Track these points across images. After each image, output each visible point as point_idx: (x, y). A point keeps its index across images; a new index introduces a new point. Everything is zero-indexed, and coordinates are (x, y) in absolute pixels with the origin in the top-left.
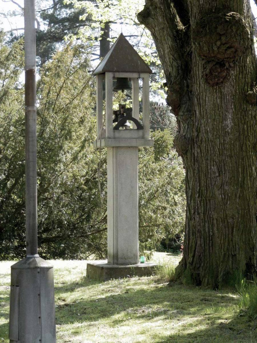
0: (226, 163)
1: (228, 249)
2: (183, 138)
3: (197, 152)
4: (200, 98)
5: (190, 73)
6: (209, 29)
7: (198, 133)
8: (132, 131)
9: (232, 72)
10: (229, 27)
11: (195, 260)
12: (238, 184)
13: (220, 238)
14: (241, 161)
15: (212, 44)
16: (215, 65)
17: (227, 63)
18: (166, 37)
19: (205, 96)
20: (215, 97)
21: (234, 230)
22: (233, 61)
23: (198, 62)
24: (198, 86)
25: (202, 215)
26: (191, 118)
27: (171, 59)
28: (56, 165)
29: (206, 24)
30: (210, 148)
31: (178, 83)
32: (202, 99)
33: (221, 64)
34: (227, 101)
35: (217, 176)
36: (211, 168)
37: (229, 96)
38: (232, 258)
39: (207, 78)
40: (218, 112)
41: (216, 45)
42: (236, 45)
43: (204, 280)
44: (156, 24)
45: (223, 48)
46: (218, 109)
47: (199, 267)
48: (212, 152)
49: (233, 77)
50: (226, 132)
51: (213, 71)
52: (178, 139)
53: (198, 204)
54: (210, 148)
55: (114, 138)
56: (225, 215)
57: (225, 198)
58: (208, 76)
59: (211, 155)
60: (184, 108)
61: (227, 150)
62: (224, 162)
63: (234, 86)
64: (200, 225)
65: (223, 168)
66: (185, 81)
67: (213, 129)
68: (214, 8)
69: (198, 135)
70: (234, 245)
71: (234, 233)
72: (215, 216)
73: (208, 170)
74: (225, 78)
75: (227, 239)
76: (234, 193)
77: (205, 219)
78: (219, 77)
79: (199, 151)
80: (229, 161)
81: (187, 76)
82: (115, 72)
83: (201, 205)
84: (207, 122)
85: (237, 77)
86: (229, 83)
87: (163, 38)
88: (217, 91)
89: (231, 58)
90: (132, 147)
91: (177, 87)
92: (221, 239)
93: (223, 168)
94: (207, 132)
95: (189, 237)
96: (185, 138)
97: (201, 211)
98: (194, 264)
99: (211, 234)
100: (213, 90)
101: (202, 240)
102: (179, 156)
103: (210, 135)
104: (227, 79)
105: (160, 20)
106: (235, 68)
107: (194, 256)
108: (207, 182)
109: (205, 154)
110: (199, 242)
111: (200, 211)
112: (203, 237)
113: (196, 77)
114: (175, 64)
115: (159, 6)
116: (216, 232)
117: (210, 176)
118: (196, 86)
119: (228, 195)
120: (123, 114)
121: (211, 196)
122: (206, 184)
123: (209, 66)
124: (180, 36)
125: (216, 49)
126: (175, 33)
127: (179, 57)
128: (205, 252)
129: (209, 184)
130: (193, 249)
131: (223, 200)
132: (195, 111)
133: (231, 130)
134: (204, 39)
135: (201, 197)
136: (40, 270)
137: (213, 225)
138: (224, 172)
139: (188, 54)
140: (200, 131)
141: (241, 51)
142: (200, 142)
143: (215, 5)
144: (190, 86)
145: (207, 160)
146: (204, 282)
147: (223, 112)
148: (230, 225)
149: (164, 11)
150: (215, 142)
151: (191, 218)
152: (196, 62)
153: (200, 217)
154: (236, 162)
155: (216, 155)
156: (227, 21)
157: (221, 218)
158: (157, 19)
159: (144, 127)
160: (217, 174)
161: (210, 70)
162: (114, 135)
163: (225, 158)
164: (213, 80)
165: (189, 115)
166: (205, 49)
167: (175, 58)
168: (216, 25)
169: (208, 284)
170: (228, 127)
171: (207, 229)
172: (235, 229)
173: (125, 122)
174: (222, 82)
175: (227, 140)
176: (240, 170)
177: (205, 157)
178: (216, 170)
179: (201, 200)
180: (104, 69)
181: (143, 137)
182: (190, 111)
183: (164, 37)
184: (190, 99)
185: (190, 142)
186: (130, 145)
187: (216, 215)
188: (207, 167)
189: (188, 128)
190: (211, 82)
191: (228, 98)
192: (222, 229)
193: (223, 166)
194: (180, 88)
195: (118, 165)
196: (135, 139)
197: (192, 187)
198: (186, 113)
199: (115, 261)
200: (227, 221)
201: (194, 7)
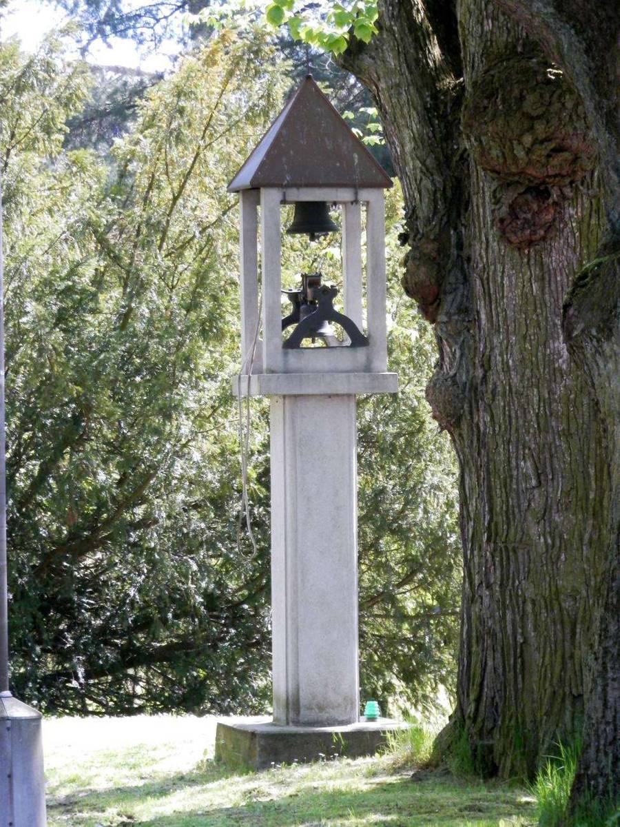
0: (556, 452)
1: (561, 680)
2: (450, 383)
3: (485, 422)
4: (488, 279)
5: (466, 210)
6: (504, 101)
7: (486, 372)
8: (337, 352)
9: (571, 212)
10: (555, 96)
11: (482, 708)
12: (587, 508)
13: (542, 650)
14: (593, 445)
15: (511, 141)
16: (524, 193)
17: (555, 188)
18: (405, 110)
19: (500, 274)
20: (526, 277)
21: (578, 630)
22: (571, 183)
23: (481, 184)
24: (484, 246)
25: (498, 589)
26: (468, 331)
27: (418, 171)
28: (168, 417)
29: (497, 89)
30: (516, 412)
31: (432, 237)
32: (495, 281)
33: (540, 191)
34: (557, 287)
35: (534, 488)
36: (517, 466)
37: (561, 275)
38: (573, 704)
39: (504, 227)
40: (534, 317)
41: (520, 143)
42: (575, 143)
43: (502, 762)
44: (382, 75)
45: (541, 151)
46: (535, 310)
47: (493, 728)
48: (521, 422)
49: (574, 225)
50: (554, 369)
51: (520, 208)
52: (435, 385)
53: (487, 561)
54: (516, 412)
55: (286, 372)
56: (553, 589)
57: (553, 545)
58: (505, 223)
59: (517, 430)
60: (449, 303)
61: (557, 418)
62: (550, 449)
63: (575, 249)
64: (492, 616)
65: (548, 464)
66: (452, 232)
67: (523, 360)
68: (521, 41)
69: (485, 377)
70: (577, 668)
71: (578, 636)
72: (530, 592)
73: (510, 470)
74: (549, 227)
75: (559, 653)
76: (576, 533)
77: (504, 603)
78: (534, 225)
79: (488, 419)
80: (564, 446)
81: (459, 216)
82: (289, 186)
83: (494, 565)
84: (508, 341)
85: (585, 225)
86: (562, 241)
87: (398, 111)
88: (532, 262)
89: (563, 176)
90: (337, 395)
91: (430, 248)
92: (544, 653)
93: (548, 464)
94: (506, 370)
95: (469, 647)
96: (455, 383)
97: (496, 578)
98: (479, 719)
99: (520, 639)
100: (522, 259)
101: (498, 655)
102: (442, 429)
103: (515, 380)
104: (557, 230)
105: (393, 63)
106: (579, 200)
107: (478, 700)
108: (508, 501)
109: (503, 429)
110: (490, 663)
111: (492, 580)
112: (499, 648)
113: (479, 223)
114: (426, 183)
115: (388, 23)
116: (533, 634)
117: (515, 486)
118: (478, 247)
119: (561, 537)
120: (313, 303)
121: (518, 539)
122: (507, 506)
123: (508, 197)
124: (442, 107)
125: (522, 153)
126: (428, 99)
127: (438, 165)
128: (505, 687)
129: (513, 506)
130: (478, 680)
131: (550, 551)
132: (478, 313)
133: (569, 365)
134: (490, 129)
135: (495, 542)
136: (12, 724)
137: (524, 616)
138: (550, 477)
139: (462, 156)
140: (490, 368)
141: (589, 158)
142: (490, 396)
143: (524, 34)
144: (466, 243)
145: (509, 442)
146: (504, 767)
147: (547, 318)
148: (566, 618)
149: (402, 39)
150: (527, 396)
151: (474, 596)
152: (478, 183)
153: (492, 596)
154: (581, 451)
155: (531, 431)
156: (549, 81)
157: (544, 597)
158: (384, 61)
159: (370, 341)
160: (534, 482)
161: (511, 206)
162: (286, 362)
163: (554, 439)
164: (519, 234)
165: (464, 321)
166: (494, 152)
167: (428, 170)
168: (522, 91)
169: (513, 772)
170: (561, 357)
171: (509, 631)
172: (578, 626)
173: (321, 325)
174: (544, 239)
175: (560, 390)
176: (592, 471)
177: (503, 437)
178: (531, 471)
179: (495, 550)
180: (255, 177)
181: (368, 368)
182: (466, 310)
183: (402, 110)
184: (466, 280)
185: (467, 394)
186: (329, 392)
187: (531, 589)
188: (509, 462)
189: (462, 355)
190: (513, 238)
191: (559, 279)
192: (546, 625)
193: (548, 460)
194: (439, 251)
195: (298, 444)
196: (344, 375)
197: (475, 514)
198: (456, 317)
199: (291, 715)
200: (560, 604)
201: (469, 37)
